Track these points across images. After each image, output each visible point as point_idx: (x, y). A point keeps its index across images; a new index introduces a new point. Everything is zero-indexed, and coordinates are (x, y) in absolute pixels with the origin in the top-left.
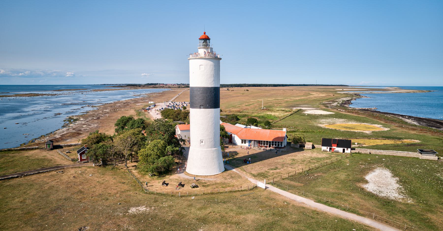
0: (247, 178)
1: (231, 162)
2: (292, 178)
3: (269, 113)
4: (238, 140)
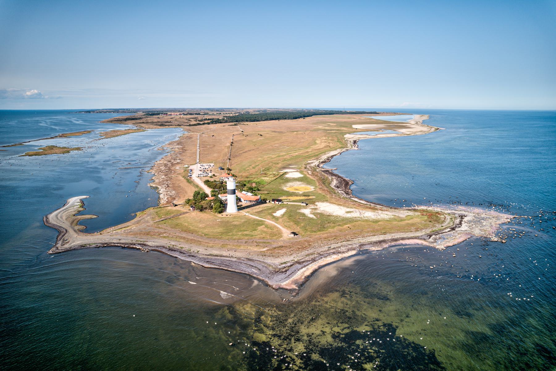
0: (243, 212)
1: (240, 208)
2: (256, 212)
3: (74, 243)
4: (242, 200)
